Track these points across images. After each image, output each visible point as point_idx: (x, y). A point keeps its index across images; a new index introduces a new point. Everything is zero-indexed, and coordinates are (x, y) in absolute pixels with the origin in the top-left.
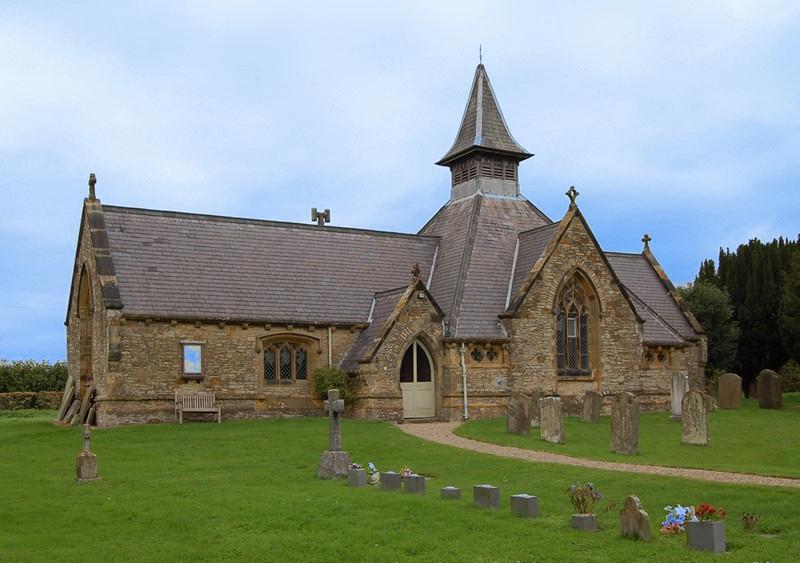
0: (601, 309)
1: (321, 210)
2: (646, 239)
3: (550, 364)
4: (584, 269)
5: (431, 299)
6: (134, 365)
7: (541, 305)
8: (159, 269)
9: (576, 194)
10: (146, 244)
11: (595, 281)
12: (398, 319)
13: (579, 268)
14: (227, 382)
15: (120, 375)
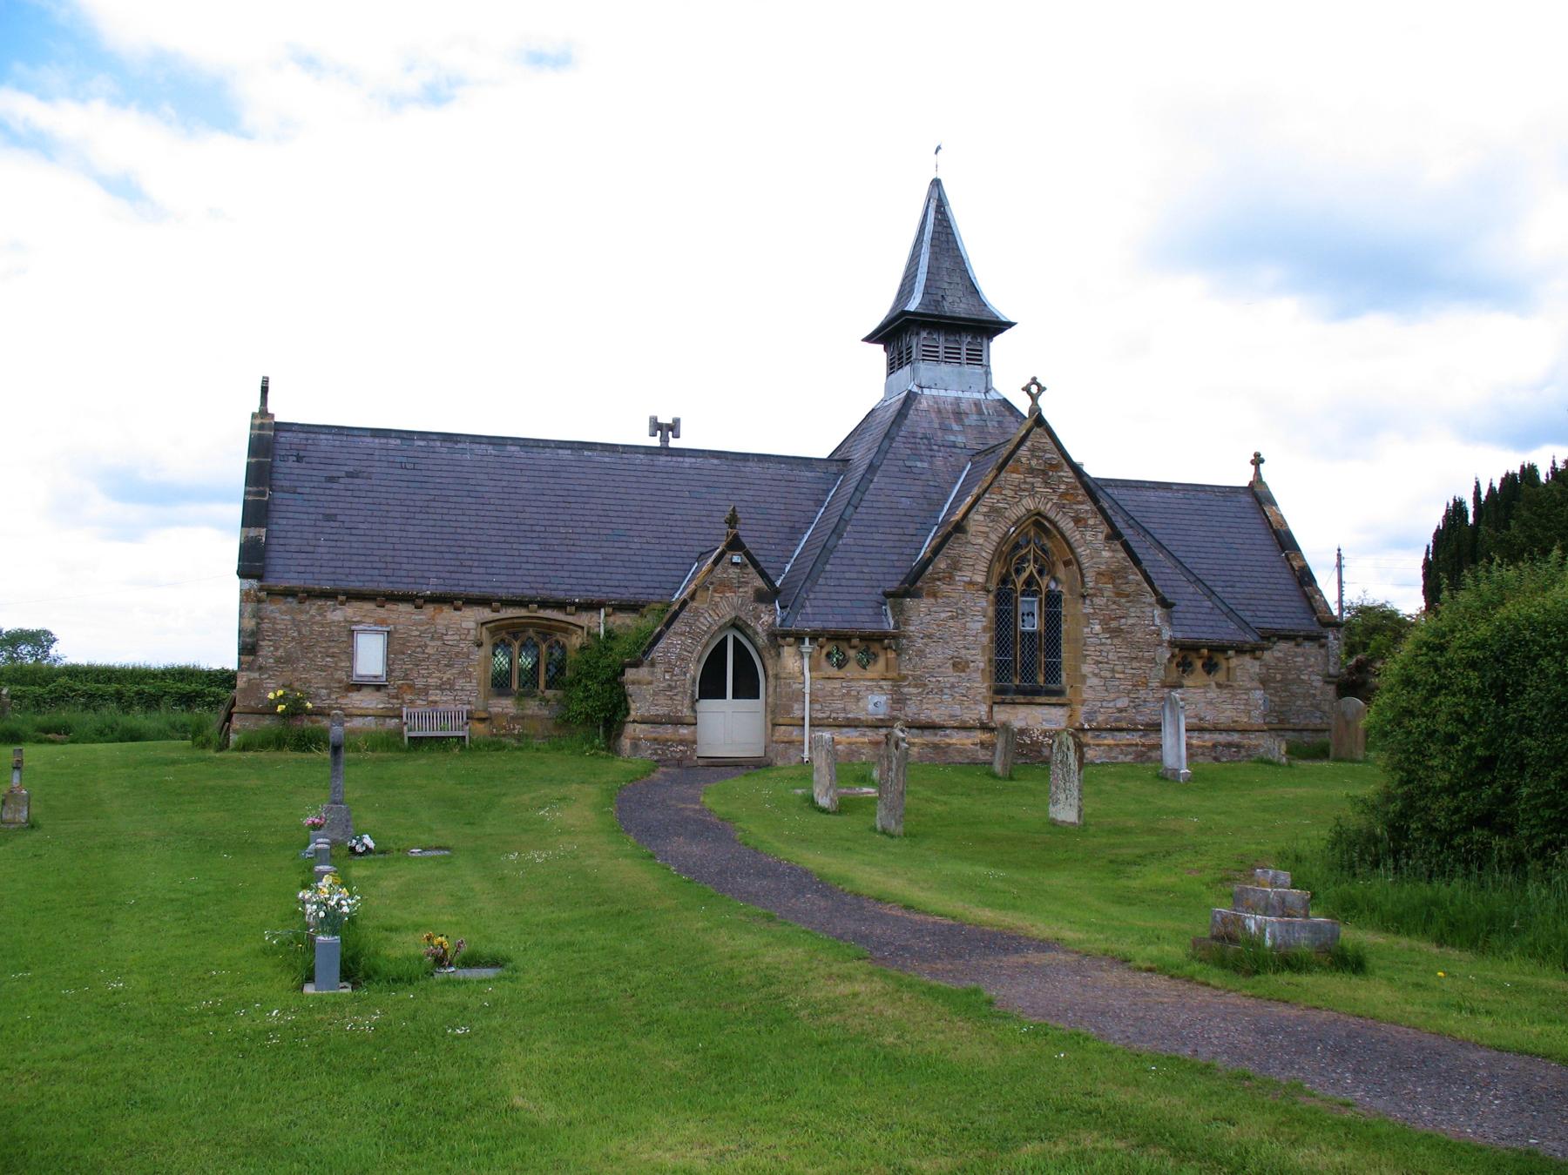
0: (1083, 583)
1: (665, 419)
2: (1257, 460)
3: (978, 676)
4: (1052, 515)
5: (755, 564)
6: (278, 660)
7: (963, 576)
8: (321, 517)
9: (1041, 389)
10: (331, 479)
11: (1074, 536)
12: (693, 596)
13: (1039, 514)
14: (425, 690)
15: (256, 675)
